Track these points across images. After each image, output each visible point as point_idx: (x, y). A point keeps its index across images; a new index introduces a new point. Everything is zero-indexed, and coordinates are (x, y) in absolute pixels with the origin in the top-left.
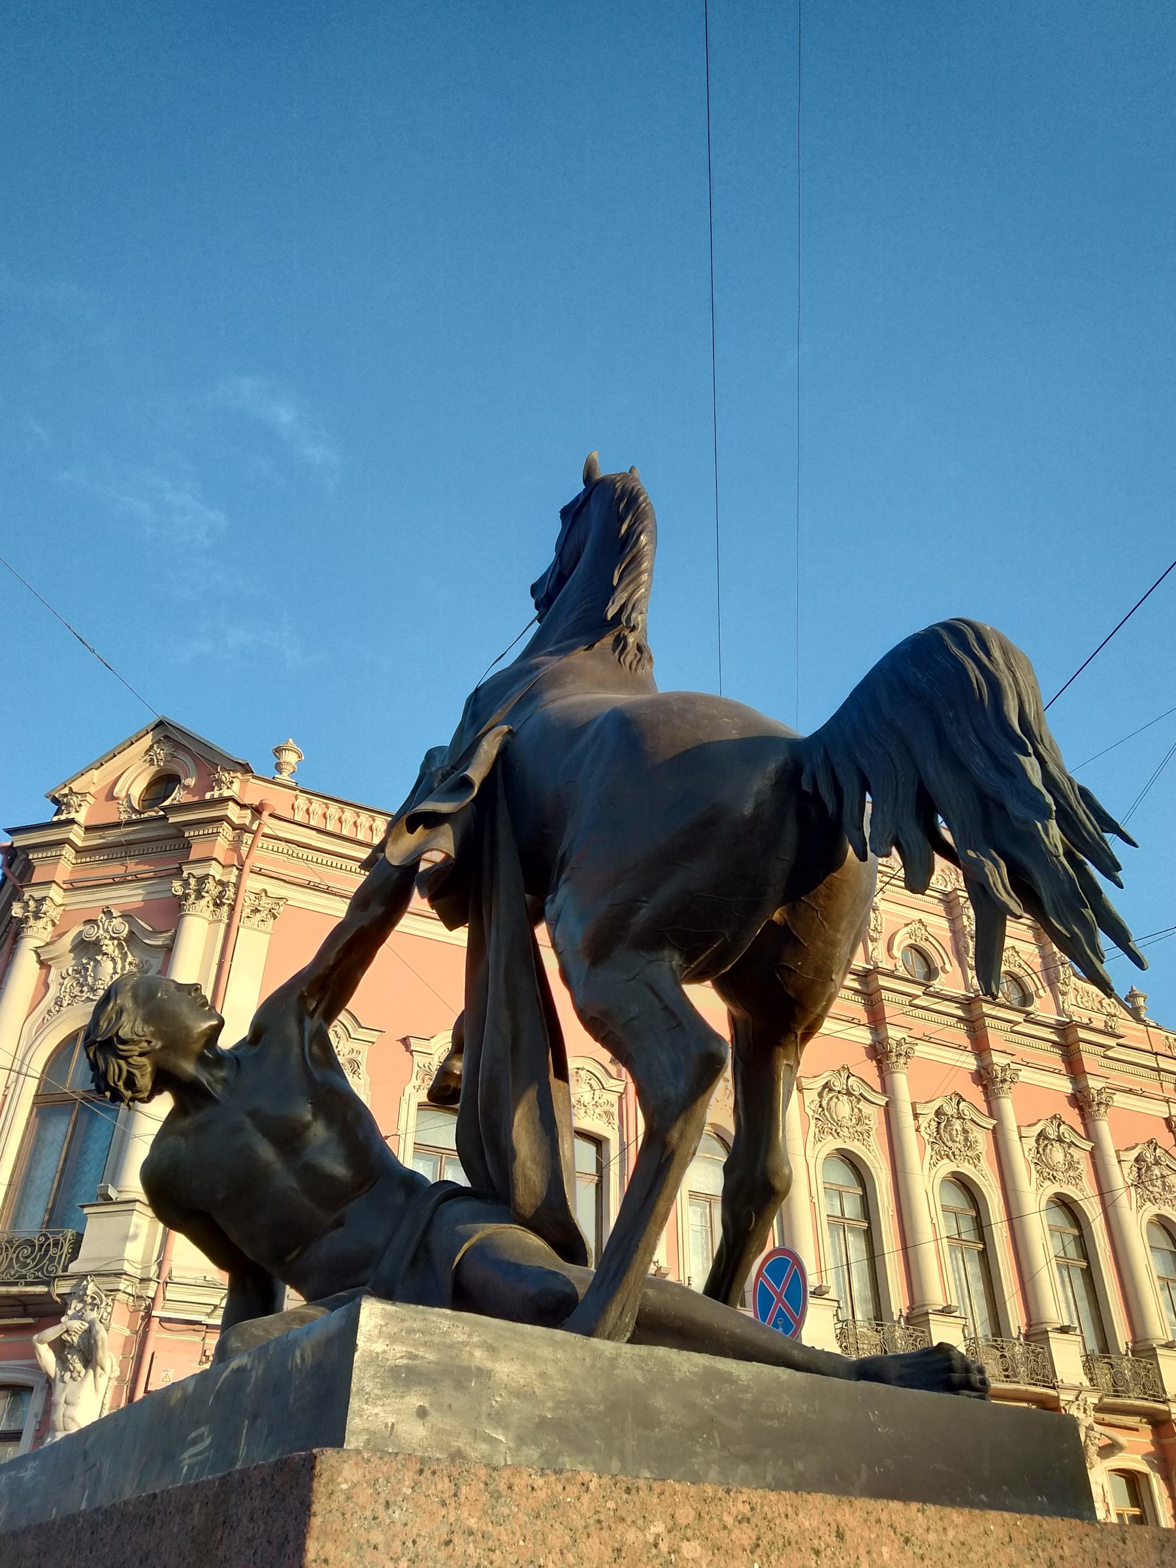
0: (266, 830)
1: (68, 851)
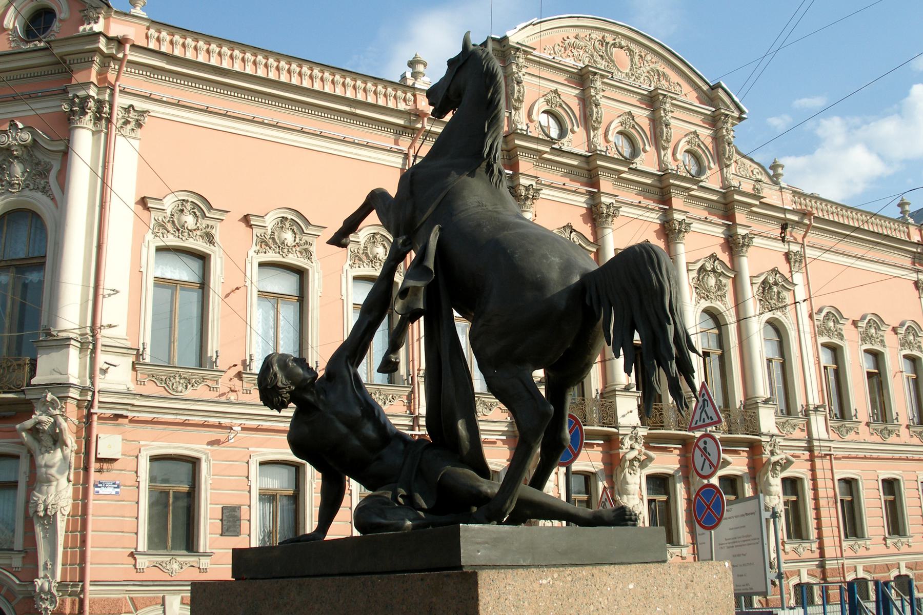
0: (130, 58)
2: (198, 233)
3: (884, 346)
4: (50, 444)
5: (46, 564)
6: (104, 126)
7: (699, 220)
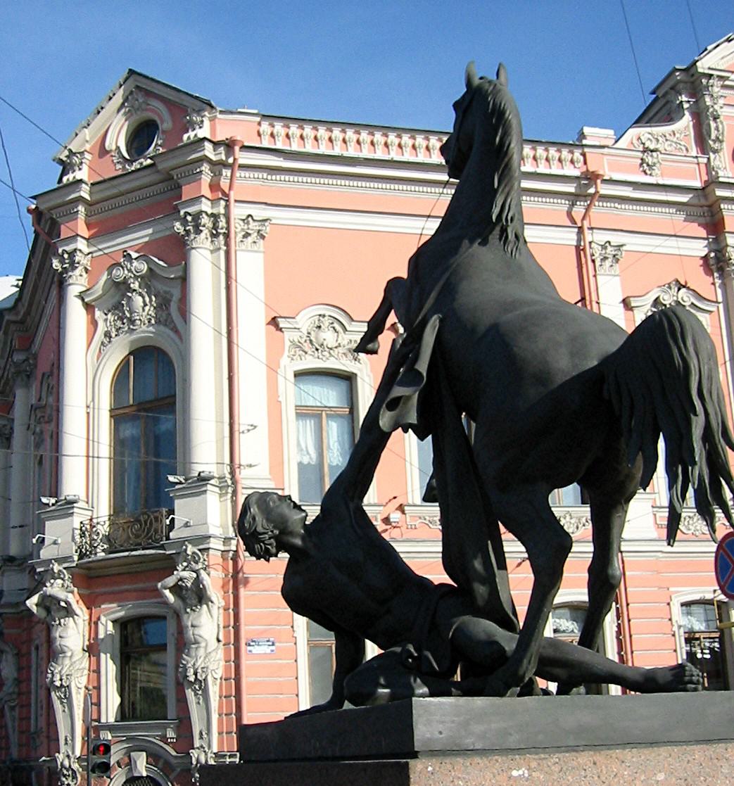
0: (241, 161)
2: (341, 350)
4: (195, 602)
5: (201, 734)
6: (223, 242)
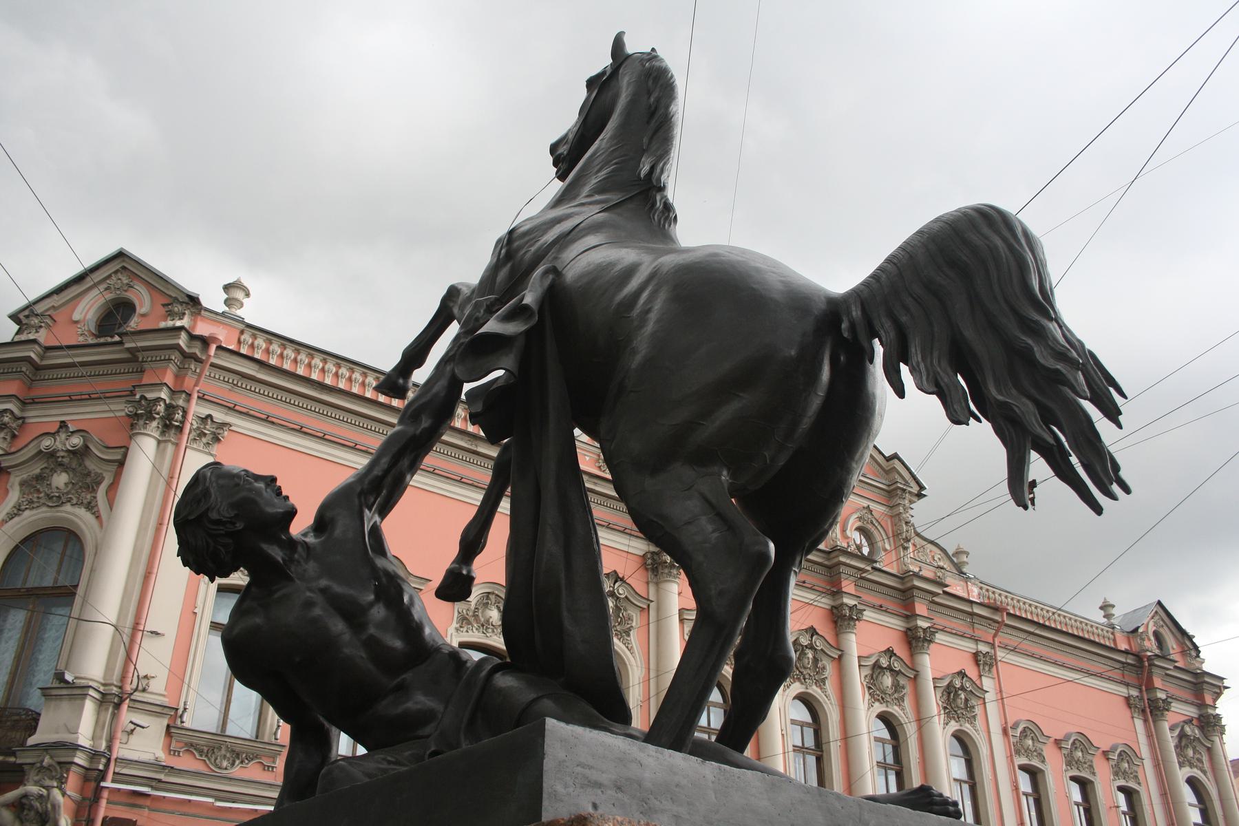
1: (175, 356)
3: (1043, 762)
7: (874, 607)
